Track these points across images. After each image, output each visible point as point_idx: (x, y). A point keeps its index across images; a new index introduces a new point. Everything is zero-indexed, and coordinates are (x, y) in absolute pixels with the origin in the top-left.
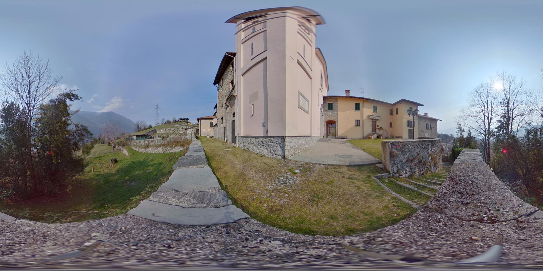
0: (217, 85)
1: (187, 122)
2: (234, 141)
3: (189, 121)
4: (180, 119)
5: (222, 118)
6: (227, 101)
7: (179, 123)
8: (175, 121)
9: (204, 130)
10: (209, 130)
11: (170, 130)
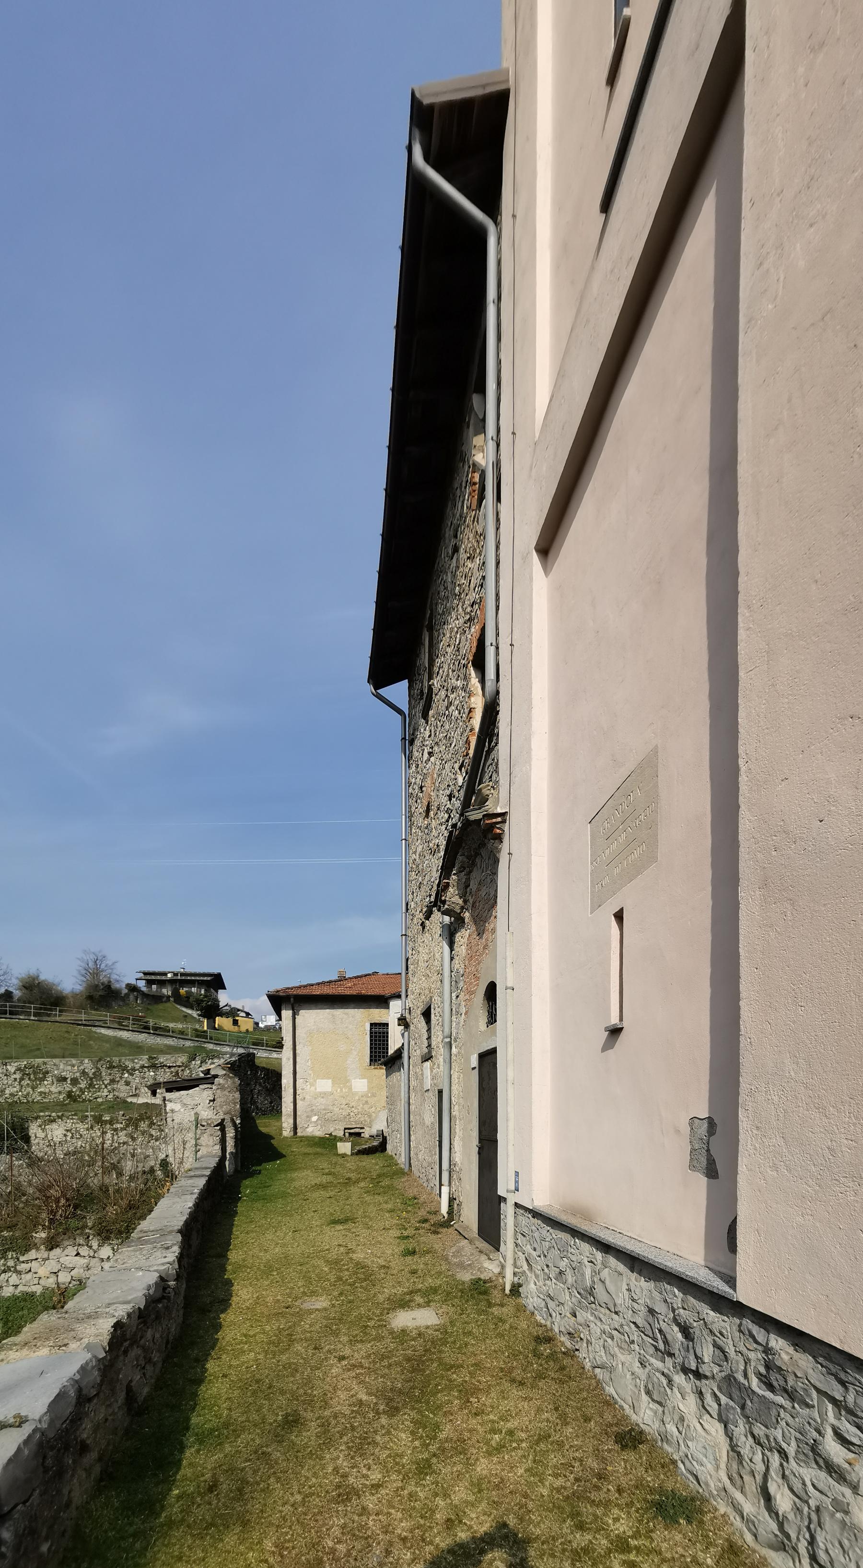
0: (399, 692)
1: (212, 1010)
2: (490, 1230)
3: (224, 998)
4: (153, 978)
5: (427, 1014)
6: (446, 870)
7: (138, 1006)
8: (103, 996)
9: (325, 1085)
10: (360, 1085)
11: (39, 1075)
